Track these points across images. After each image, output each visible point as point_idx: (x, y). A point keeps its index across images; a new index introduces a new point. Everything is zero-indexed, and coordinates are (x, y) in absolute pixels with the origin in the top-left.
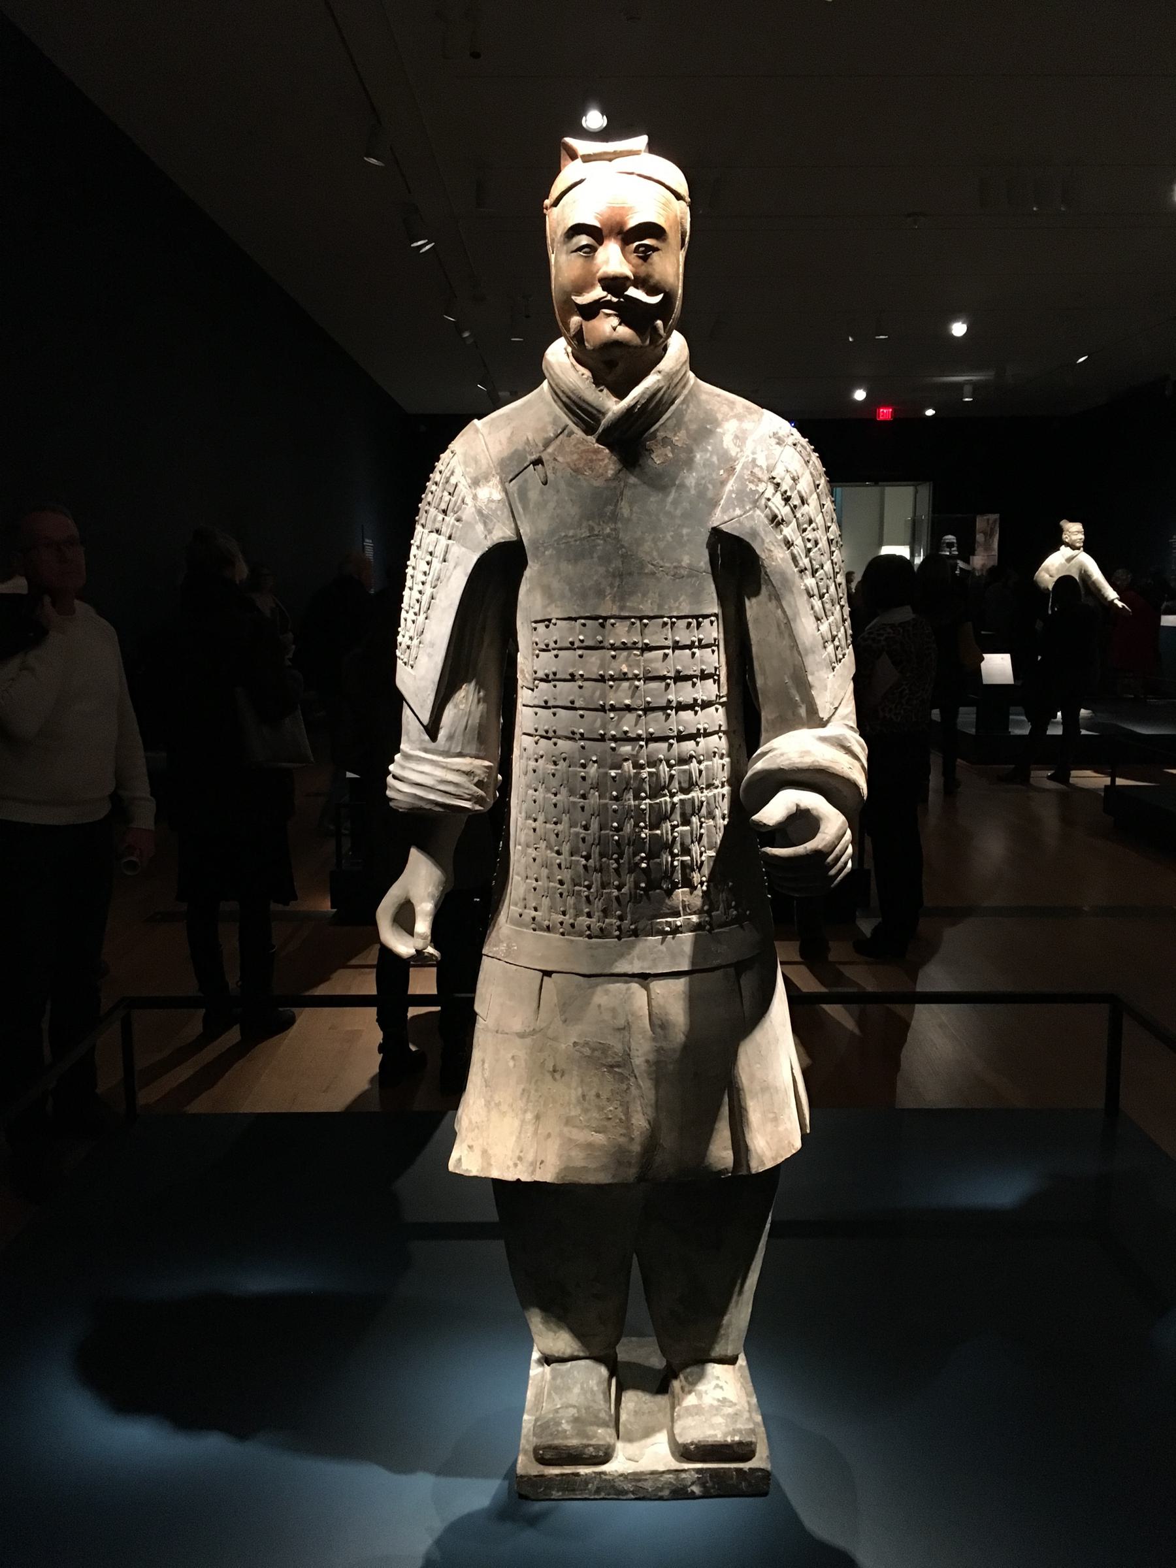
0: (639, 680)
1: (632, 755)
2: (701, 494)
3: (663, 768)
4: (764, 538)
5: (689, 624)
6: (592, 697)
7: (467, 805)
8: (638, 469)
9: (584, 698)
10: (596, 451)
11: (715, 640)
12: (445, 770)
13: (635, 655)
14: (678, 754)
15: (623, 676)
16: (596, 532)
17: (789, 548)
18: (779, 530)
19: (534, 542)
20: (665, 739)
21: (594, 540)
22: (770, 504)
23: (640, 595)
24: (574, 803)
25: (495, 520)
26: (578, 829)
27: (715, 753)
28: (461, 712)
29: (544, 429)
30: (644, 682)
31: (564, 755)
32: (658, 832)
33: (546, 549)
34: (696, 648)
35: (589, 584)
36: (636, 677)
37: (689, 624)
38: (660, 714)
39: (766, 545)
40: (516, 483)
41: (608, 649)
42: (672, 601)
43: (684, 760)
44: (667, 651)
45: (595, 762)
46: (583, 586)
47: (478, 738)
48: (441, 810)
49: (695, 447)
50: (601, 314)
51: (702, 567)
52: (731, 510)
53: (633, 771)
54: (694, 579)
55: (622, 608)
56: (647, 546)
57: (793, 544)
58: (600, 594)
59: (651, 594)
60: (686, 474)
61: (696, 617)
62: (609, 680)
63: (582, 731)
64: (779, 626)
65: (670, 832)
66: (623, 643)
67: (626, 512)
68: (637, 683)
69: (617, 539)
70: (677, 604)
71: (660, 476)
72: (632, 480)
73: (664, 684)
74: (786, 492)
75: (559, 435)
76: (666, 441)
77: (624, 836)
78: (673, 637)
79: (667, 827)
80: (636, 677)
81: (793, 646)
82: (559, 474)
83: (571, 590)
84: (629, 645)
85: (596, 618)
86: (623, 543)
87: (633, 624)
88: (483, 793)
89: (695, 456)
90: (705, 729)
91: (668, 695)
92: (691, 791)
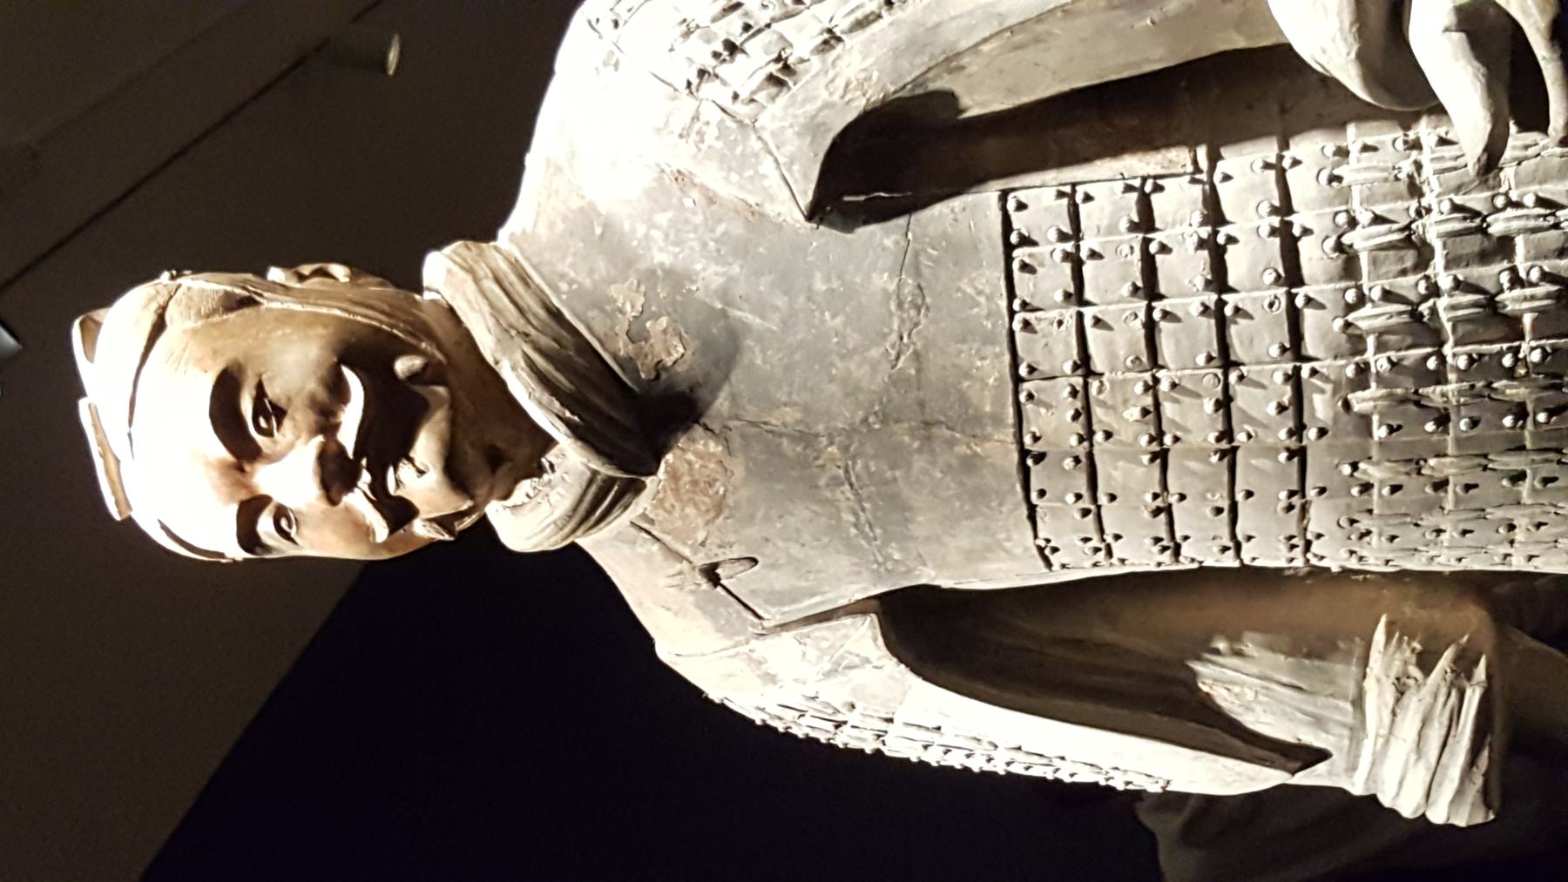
0: (1156, 380)
1: (1335, 392)
2: (742, 250)
3: (1365, 319)
4: (819, 103)
5: (1025, 267)
6: (1203, 478)
7: (1473, 697)
8: (703, 394)
9: (1208, 491)
10: (674, 476)
11: (1061, 195)
12: (1393, 739)
13: (1100, 391)
14: (1330, 280)
15: (1150, 417)
16: (841, 472)
17: (839, 40)
18: (800, 68)
19: (878, 577)
20: (1294, 317)
21: (858, 477)
22: (744, 95)
23: (966, 384)
24: (1457, 501)
25: (841, 652)
26: (1524, 488)
27: (1334, 178)
28: (1261, 698)
29: (649, 558)
30: (1162, 367)
31: (1344, 522)
32: (1527, 320)
33: (888, 558)
34: (1078, 248)
35: (952, 485)
36: (1152, 387)
37: (1025, 267)
38: (1233, 331)
39: (836, 98)
40: (760, 608)
41: (1092, 445)
42: (976, 310)
43: (1349, 266)
44: (1088, 322)
45: (1355, 466)
46: (958, 497)
47: (1321, 657)
48: (1485, 753)
49: (643, 266)
50: (400, 493)
51: (897, 243)
52: (766, 183)
53: (1374, 390)
54: (924, 260)
55: (998, 421)
56: (859, 371)
57: (830, 31)
58: (970, 464)
59: (962, 360)
60: (700, 284)
61: (1009, 248)
62: (1161, 444)
63: (1283, 495)
64: (1020, 47)
65: (1528, 291)
66: (1076, 417)
67: (791, 415)
68: (1164, 386)
69: (852, 431)
70: (982, 299)
71: (707, 346)
72: (722, 404)
73: (1163, 325)
74: (716, 55)
75: (654, 536)
76: (637, 335)
77: (1538, 401)
78: (1055, 306)
79: (1515, 300)
80: (1152, 387)
81: (1064, 11)
82: (732, 538)
83: (970, 517)
84: (1079, 404)
85: (1025, 473)
86: (857, 421)
87: (1030, 396)
88: (1449, 654)
89: (662, 265)
90: (1275, 211)
91: (1188, 313)
92: (1424, 243)
